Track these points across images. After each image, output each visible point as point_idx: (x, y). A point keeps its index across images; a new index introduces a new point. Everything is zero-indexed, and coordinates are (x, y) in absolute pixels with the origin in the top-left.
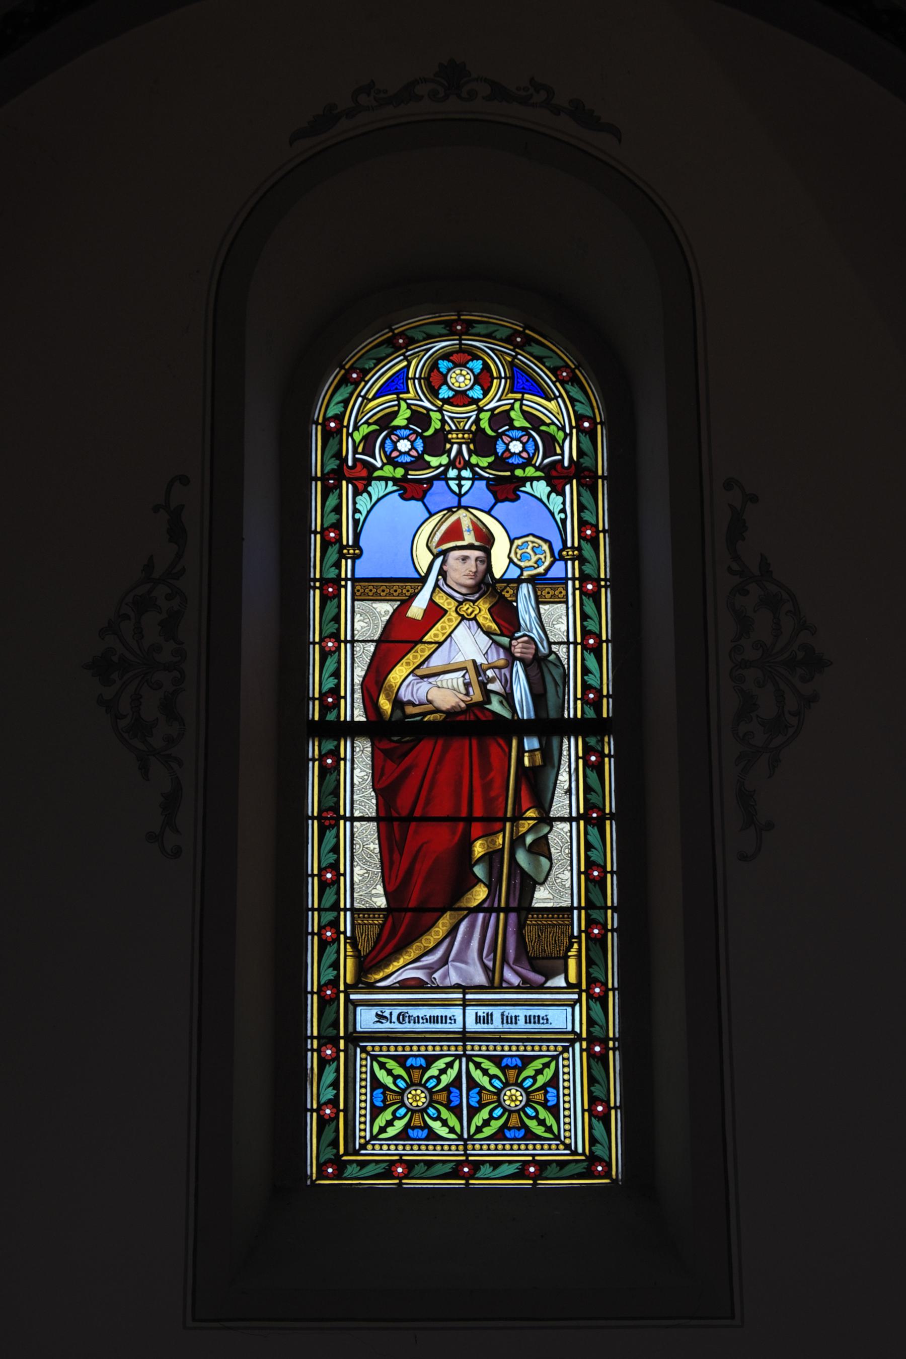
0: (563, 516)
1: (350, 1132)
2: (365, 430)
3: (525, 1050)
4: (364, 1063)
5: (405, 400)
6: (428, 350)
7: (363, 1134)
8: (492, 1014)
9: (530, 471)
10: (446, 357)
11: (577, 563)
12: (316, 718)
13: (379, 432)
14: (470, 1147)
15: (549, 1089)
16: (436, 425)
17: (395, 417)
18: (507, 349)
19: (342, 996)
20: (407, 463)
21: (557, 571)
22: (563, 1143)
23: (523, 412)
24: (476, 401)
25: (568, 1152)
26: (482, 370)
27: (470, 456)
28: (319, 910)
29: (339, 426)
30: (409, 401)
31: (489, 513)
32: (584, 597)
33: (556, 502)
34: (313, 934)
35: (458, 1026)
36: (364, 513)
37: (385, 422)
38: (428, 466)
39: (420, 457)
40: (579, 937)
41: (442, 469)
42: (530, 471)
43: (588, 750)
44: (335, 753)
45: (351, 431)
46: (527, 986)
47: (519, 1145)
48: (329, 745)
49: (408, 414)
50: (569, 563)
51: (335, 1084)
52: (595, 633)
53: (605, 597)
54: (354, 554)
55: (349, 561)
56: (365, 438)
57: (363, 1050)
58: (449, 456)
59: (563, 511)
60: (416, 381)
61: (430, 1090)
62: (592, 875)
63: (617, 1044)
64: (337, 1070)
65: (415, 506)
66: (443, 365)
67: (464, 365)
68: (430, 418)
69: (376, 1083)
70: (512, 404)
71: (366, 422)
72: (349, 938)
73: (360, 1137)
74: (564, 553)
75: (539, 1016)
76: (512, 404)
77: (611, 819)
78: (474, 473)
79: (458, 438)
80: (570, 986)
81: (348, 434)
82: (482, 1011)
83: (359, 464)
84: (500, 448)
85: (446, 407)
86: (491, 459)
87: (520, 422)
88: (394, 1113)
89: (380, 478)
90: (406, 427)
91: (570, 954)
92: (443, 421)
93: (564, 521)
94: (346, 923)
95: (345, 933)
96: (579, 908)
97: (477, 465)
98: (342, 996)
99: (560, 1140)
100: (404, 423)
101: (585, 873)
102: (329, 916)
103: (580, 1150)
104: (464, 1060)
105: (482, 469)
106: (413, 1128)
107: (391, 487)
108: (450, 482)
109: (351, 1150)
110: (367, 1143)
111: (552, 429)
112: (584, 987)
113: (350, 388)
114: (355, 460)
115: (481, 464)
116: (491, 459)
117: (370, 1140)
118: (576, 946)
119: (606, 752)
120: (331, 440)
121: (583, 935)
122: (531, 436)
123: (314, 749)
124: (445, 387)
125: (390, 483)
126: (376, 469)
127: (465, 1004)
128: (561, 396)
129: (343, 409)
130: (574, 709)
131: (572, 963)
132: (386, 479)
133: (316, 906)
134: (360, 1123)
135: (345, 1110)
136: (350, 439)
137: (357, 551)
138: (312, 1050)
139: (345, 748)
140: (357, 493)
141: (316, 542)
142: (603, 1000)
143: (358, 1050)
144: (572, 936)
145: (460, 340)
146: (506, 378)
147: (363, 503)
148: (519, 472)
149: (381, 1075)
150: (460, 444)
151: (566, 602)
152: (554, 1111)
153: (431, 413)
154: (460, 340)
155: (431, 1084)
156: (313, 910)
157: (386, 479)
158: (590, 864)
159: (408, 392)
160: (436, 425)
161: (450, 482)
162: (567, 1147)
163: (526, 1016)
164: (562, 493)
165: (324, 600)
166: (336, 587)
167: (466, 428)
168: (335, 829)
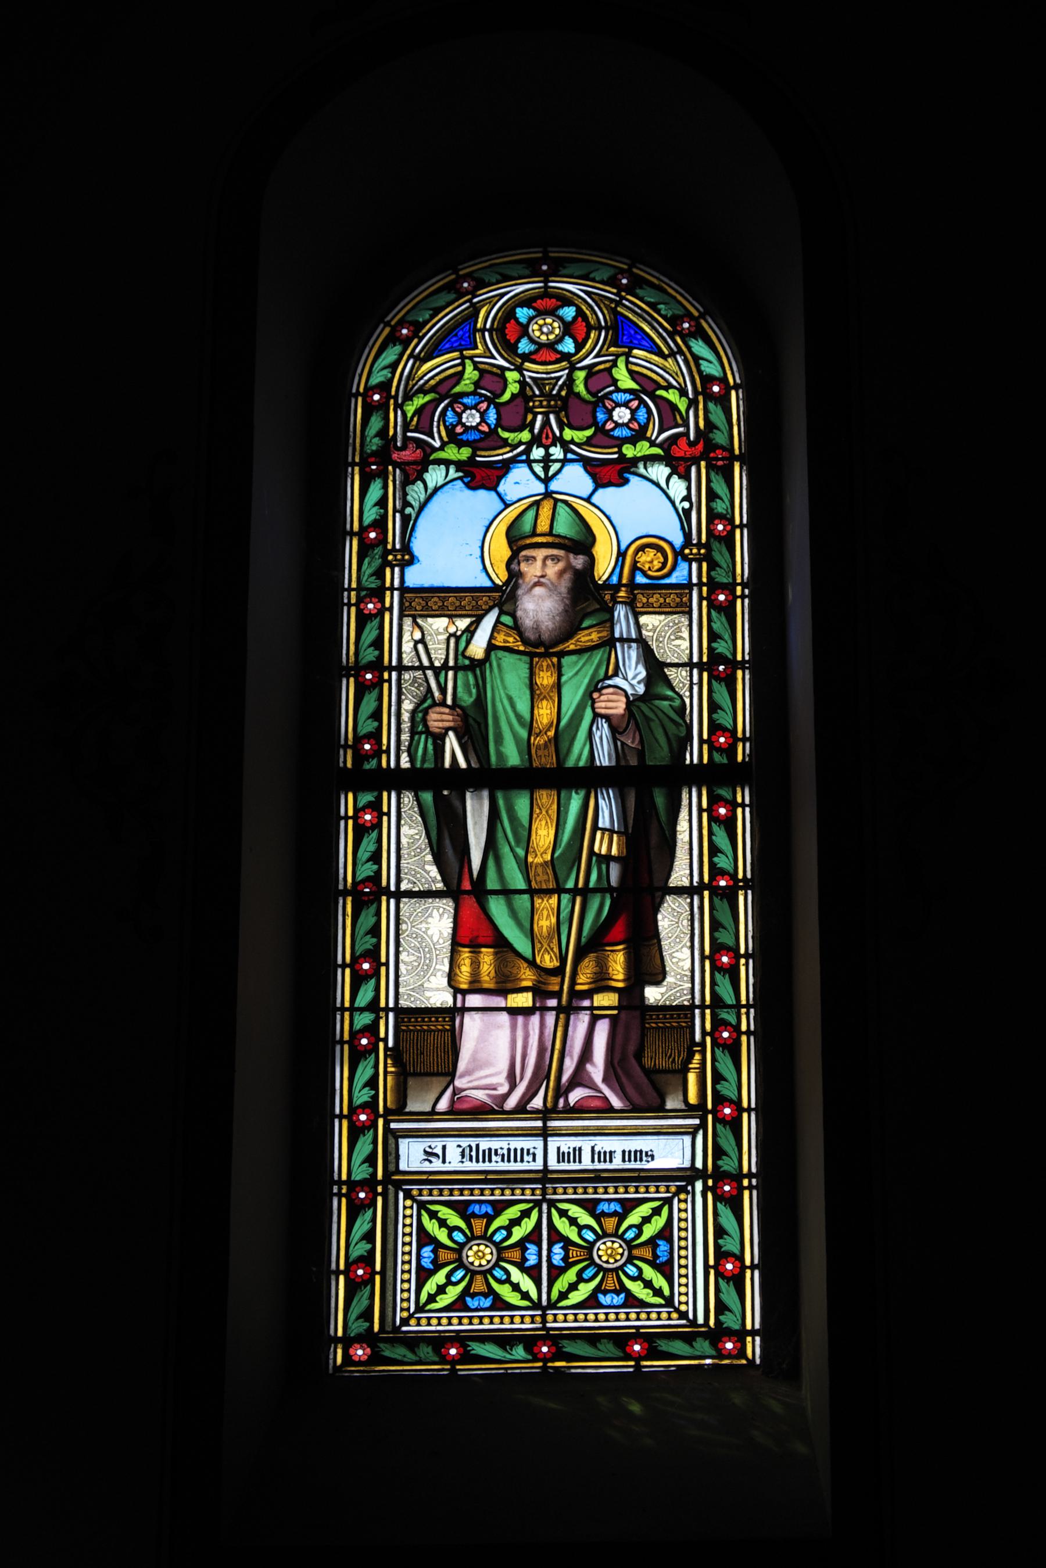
0: (686, 505)
1: (390, 1246)
2: (420, 401)
3: (626, 1192)
4: (408, 1212)
5: (471, 358)
6: (502, 295)
7: (405, 1305)
8: (580, 1149)
9: (643, 448)
10: (526, 302)
11: (705, 565)
12: (349, 765)
13: (436, 403)
14: (550, 1318)
15: (660, 1242)
17: (458, 383)
18: (610, 293)
19: (381, 1122)
20: (475, 441)
21: (679, 576)
22: (677, 1310)
23: (631, 372)
24: (566, 357)
25: (684, 1322)
27: (561, 430)
28: (352, 1009)
29: (371, 1195)
31: (588, 500)
32: (720, 1280)
33: (678, 488)
34: (341, 1117)
35: (539, 1165)
39: (493, 432)
40: (703, 1044)
41: (522, 448)
42: (643, 448)
43: (714, 800)
44: (376, 806)
45: (400, 401)
46: (634, 1109)
47: (617, 1314)
48: (366, 798)
49: (475, 375)
50: (694, 565)
51: (369, 1237)
52: (733, 1255)
53: (742, 609)
54: (699, 554)
55: (397, 569)
56: (419, 412)
57: (408, 1195)
59: (687, 498)
60: (487, 334)
61: (497, 1245)
62: (718, 955)
63: (747, 591)
64: (375, 1142)
65: (484, 496)
66: (523, 314)
67: (552, 313)
68: (505, 380)
69: (425, 1238)
72: (390, 1049)
73: (402, 1310)
74: (687, 551)
75: (641, 1151)
77: (745, 888)
78: (566, 450)
79: (542, 407)
80: (690, 1108)
81: (397, 406)
83: (412, 446)
84: (601, 416)
85: (527, 365)
86: (589, 433)
87: (626, 382)
88: (448, 1276)
89: (439, 462)
90: (474, 393)
91: (691, 1066)
92: (523, 383)
93: (687, 513)
94: (387, 1028)
95: (385, 1040)
96: (703, 1007)
97: (572, 442)
98: (381, 1122)
99: (674, 1307)
100: (471, 388)
101: (710, 958)
102: (364, 1019)
103: (701, 1320)
104: (545, 1207)
105: (578, 445)
106: (473, 1296)
107: (453, 473)
108: (534, 465)
109: (389, 1328)
110: (411, 1316)
111: (672, 396)
112: (710, 1106)
113: (398, 349)
114: (405, 439)
115: (577, 440)
116: (589, 433)
117: (414, 1313)
118: (697, 1057)
119: (739, 800)
120: (363, 913)
121: (708, 1039)
123: (348, 804)
125: (452, 469)
126: (435, 450)
127: (545, 1134)
128: (680, 352)
129: (390, 375)
130: (695, 754)
131: (692, 1078)
132: (447, 463)
133: (347, 1004)
134: (404, 1244)
135: (383, 1273)
136: (399, 412)
137: (407, 557)
138: (340, 1195)
139: (390, 800)
140: (407, 481)
141: (353, 547)
142: (735, 1126)
143: (401, 1195)
144: (694, 1043)
145: (546, 282)
148: (629, 451)
149: (431, 1226)
150: (546, 415)
151: (690, 613)
152: (666, 1269)
153: (508, 374)
154: (546, 282)
155: (498, 1273)
156: (343, 1009)
158: (717, 947)
159: (476, 348)
160: (513, 388)
161: (534, 465)
162: (683, 1315)
163: (624, 1152)
164: (686, 477)
165: (363, 620)
166: (375, 814)
168: (375, 905)
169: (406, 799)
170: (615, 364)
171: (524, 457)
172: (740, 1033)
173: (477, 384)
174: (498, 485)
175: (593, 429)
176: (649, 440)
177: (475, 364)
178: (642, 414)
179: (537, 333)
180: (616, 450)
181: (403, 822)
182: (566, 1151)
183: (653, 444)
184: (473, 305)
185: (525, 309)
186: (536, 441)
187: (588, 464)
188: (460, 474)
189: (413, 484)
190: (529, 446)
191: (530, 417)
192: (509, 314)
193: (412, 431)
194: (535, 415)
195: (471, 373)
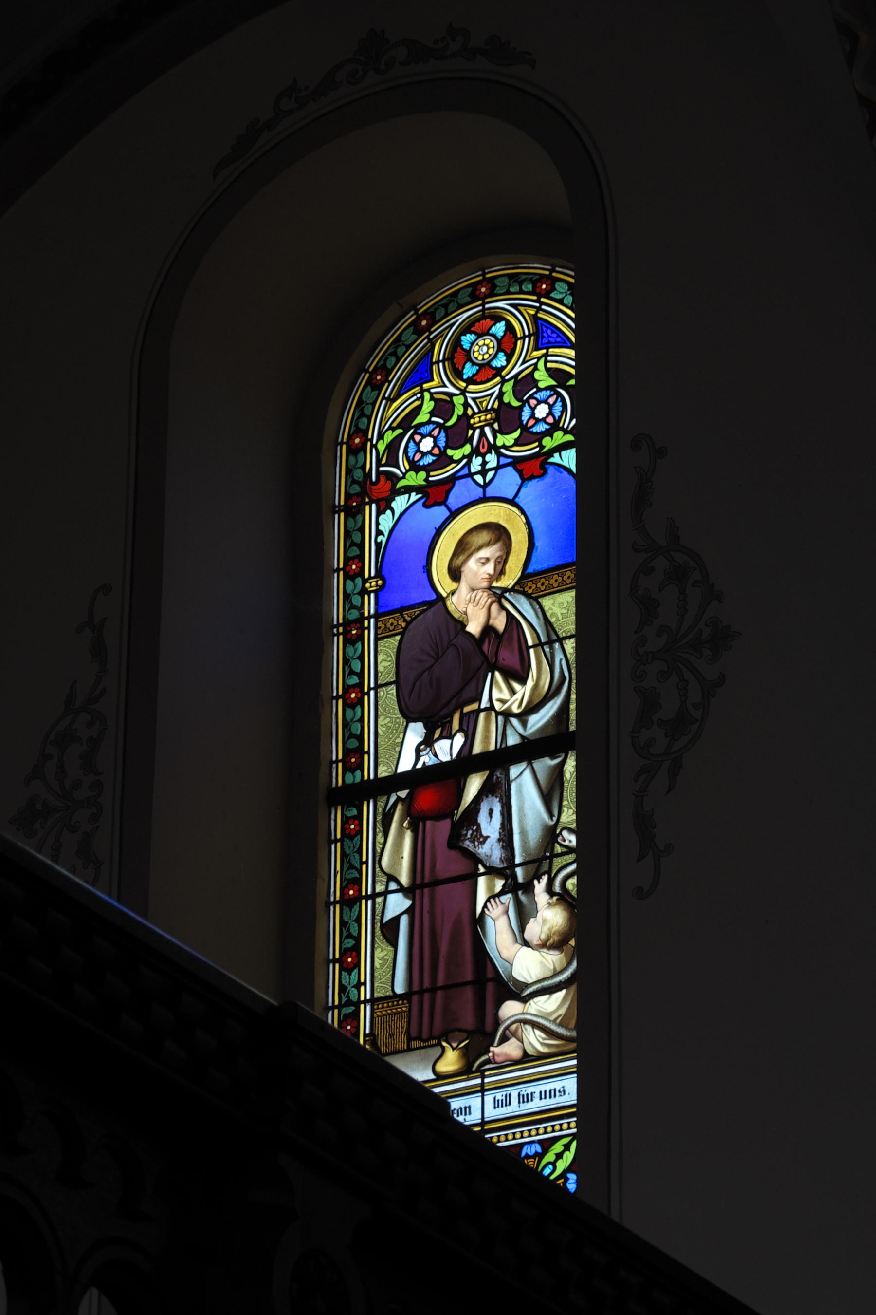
2: (389, 436)
5: (428, 390)
9: (559, 437)
10: (467, 329)
16: (459, 411)
17: (418, 414)
23: (548, 370)
24: (499, 371)
26: (505, 332)
27: (495, 438)
30: (432, 391)
36: (386, 534)
37: (407, 423)
38: (451, 460)
39: (443, 453)
41: (465, 461)
58: (471, 444)
70: (536, 365)
71: (390, 428)
76: (536, 365)
78: (499, 455)
79: (480, 422)
81: (372, 446)
82: (500, 1095)
83: (382, 478)
84: (526, 415)
86: (517, 434)
92: (466, 405)
114: (378, 473)
115: (507, 444)
116: (517, 434)
122: (560, 395)
124: (468, 365)
125: (413, 494)
127: (482, 1090)
132: (408, 490)
140: (380, 512)
146: (530, 336)
147: (386, 522)
157: (408, 490)
159: (433, 380)
160: (459, 411)
167: (489, 407)
169: (382, 693)
170: (536, 368)
171: (465, 471)
172: (347, 443)
173: (432, 413)
174: (447, 498)
175: (519, 431)
176: (562, 429)
177: (431, 394)
178: (558, 408)
179: (487, 342)
180: (537, 444)
181: (376, 946)
182: (500, 1099)
183: (566, 432)
184: (430, 340)
185: (468, 335)
186: (476, 452)
187: (516, 463)
188: (420, 496)
189: (384, 513)
190: (469, 457)
191: (470, 432)
192: (456, 343)
193: (384, 465)
194: (474, 429)
195: (428, 406)
